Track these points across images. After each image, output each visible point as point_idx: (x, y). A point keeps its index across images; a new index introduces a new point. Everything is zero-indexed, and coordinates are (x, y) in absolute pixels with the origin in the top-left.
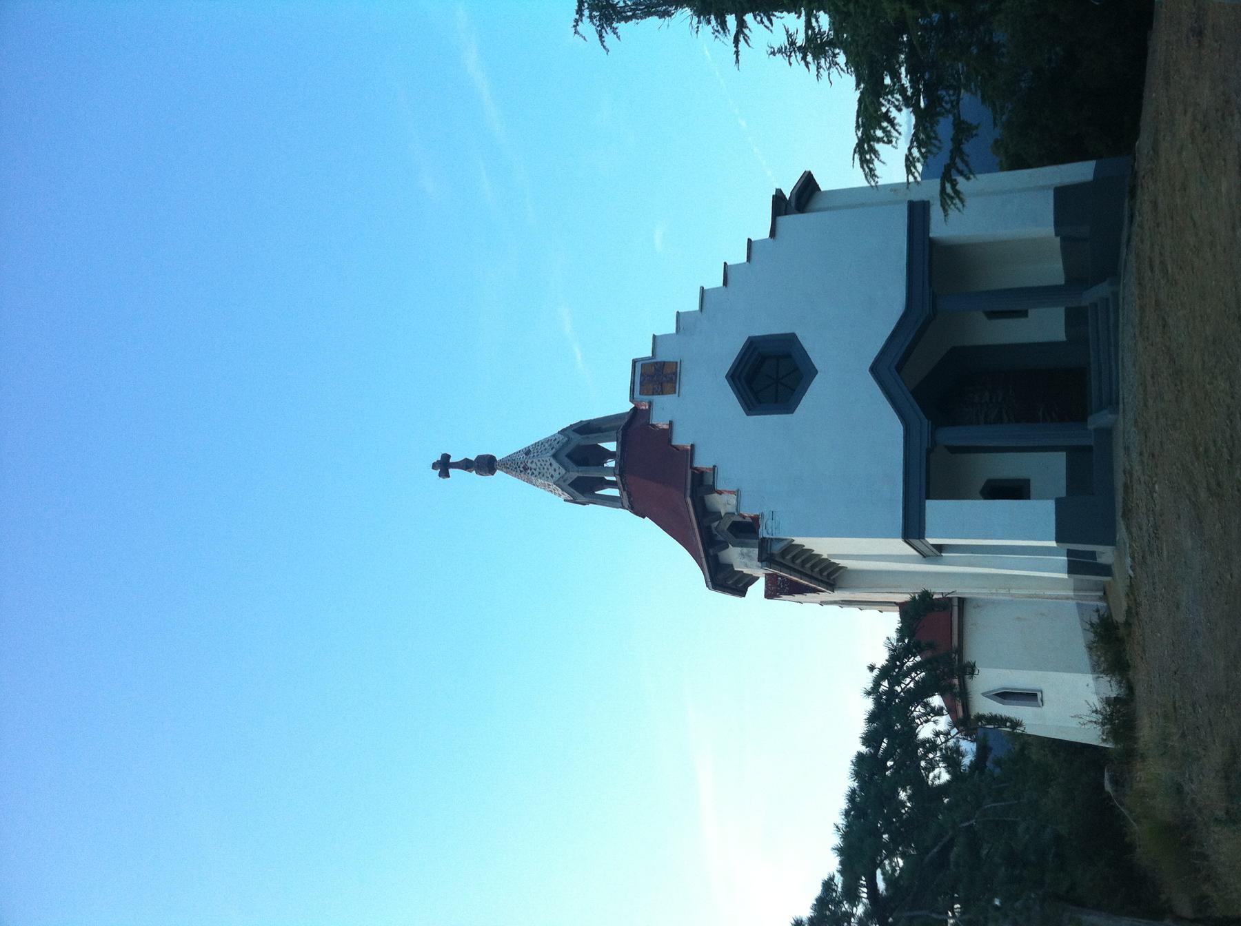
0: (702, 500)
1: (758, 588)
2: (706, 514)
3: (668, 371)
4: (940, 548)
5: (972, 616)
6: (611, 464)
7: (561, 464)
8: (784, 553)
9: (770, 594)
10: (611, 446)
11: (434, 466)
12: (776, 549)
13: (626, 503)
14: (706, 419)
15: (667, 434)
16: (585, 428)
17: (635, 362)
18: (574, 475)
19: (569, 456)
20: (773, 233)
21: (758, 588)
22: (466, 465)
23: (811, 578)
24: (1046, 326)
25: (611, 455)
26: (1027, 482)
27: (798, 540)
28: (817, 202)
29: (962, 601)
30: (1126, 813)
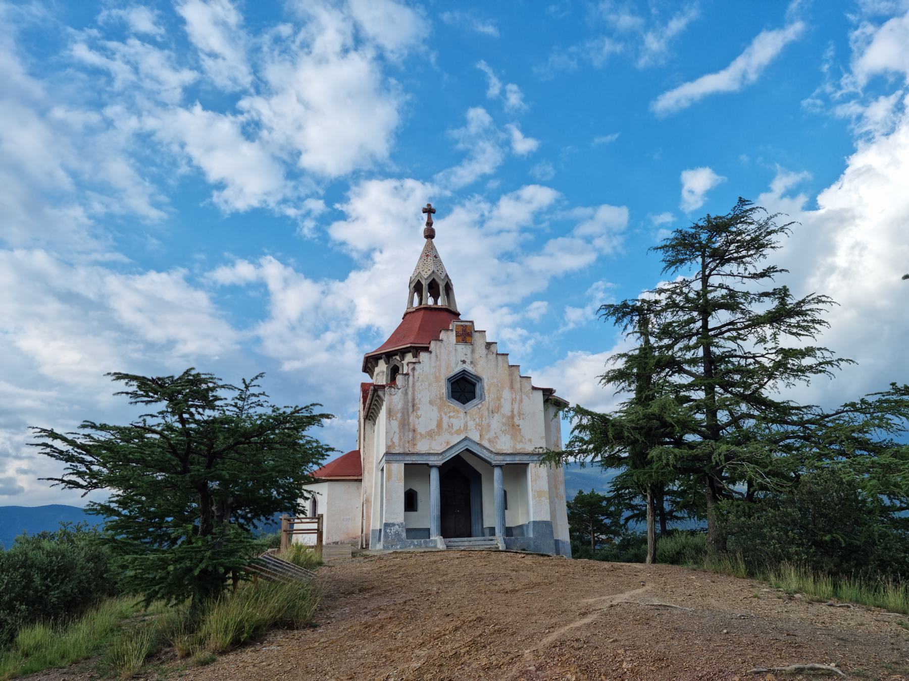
0: (409, 352)
1: (366, 378)
2: (403, 353)
3: (468, 338)
4: (382, 470)
5: (353, 485)
6: (430, 301)
7: (430, 276)
8: (378, 396)
9: (365, 387)
10: (440, 303)
11: (429, 205)
12: (380, 393)
13: (409, 310)
14: (447, 356)
15: (437, 339)
16: (448, 288)
17: (472, 322)
18: (423, 282)
19: (434, 279)
20: (534, 388)
21: (366, 378)
22: (429, 224)
23: (369, 408)
24: (490, 516)
25: (436, 302)
26: (416, 510)
27: (384, 403)
28: (552, 410)
29: (361, 480)
30: (297, 364)
